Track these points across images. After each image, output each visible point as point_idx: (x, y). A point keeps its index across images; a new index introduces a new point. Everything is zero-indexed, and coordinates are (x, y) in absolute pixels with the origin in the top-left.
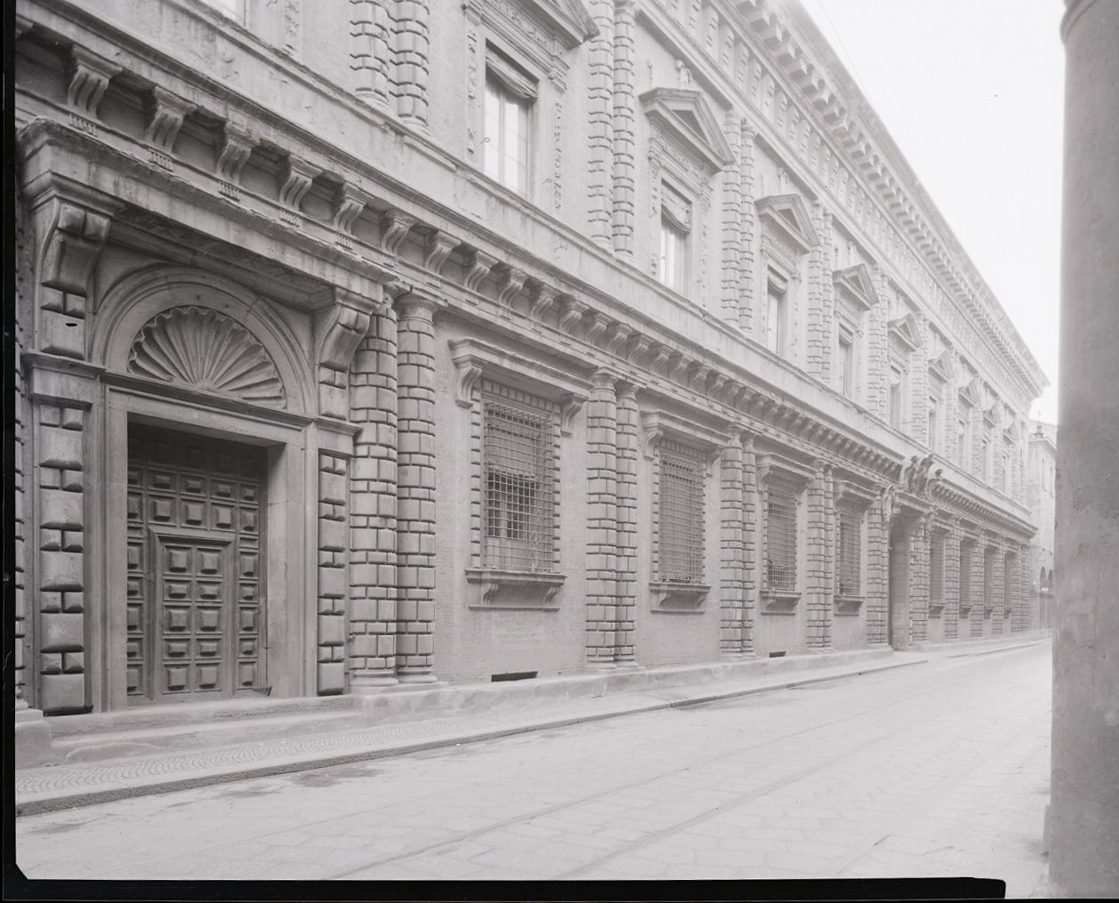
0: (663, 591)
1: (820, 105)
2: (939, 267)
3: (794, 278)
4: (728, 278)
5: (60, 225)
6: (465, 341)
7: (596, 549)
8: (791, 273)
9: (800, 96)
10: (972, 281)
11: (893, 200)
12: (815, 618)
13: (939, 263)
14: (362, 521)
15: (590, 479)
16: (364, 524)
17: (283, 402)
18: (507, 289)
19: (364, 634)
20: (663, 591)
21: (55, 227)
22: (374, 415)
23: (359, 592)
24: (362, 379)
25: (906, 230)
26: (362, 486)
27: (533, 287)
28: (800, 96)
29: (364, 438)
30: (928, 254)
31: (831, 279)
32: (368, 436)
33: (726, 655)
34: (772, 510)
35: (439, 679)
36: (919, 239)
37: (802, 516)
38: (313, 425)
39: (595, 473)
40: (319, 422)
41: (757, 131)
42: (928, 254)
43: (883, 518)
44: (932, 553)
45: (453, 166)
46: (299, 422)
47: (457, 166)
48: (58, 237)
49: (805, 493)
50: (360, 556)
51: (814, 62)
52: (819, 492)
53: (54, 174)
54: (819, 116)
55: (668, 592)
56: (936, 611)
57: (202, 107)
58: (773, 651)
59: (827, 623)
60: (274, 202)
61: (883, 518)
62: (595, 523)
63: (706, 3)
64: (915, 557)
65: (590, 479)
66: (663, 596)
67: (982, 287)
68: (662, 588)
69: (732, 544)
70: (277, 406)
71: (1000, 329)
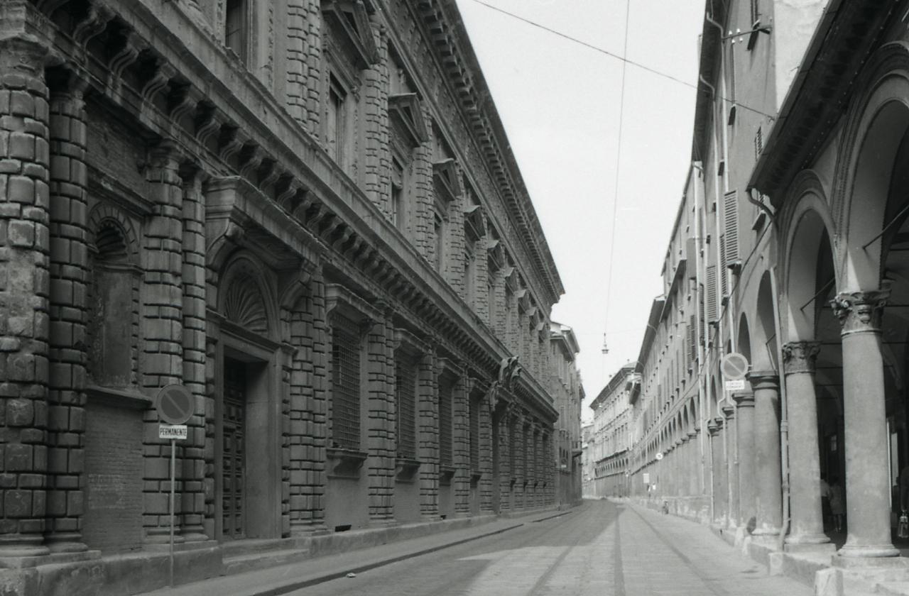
0: (337, 458)
1: (464, 94)
2: (509, 200)
3: (353, 93)
4: (420, 224)
5: (228, 234)
6: (336, 287)
7: (376, 433)
8: (443, 216)
9: (453, 88)
10: (528, 215)
11: (493, 158)
12: (461, 488)
13: (512, 202)
14: (297, 415)
15: (370, 380)
16: (299, 417)
17: (267, 333)
18: (207, 127)
19: (157, 492)
20: (337, 458)
21: (224, 235)
22: (305, 341)
23: (295, 465)
24: (296, 317)
25: (497, 178)
26: (297, 390)
27: (229, 130)
28: (453, 88)
29: (299, 357)
30: (506, 195)
31: (386, 103)
32: (301, 356)
33: (374, 521)
34: (336, 352)
35: (91, 547)
36: (503, 185)
37: (365, 366)
38: (280, 349)
39: (374, 377)
40: (283, 348)
41: (389, 36)
42: (506, 195)
43: (490, 408)
44: (440, 403)
45: (331, 167)
46: (272, 346)
47: (334, 168)
48: (223, 240)
49: (367, 338)
50: (296, 439)
51: (465, 67)
52: (381, 339)
53: (235, 207)
54: (461, 101)
55: (342, 458)
56: (350, 466)
57: (153, 48)
58: (339, 525)
59: (319, 490)
60: (103, 65)
61: (490, 408)
62: (375, 414)
63: (403, 1)
64: (502, 439)
65: (370, 380)
66: (337, 462)
67: (534, 220)
68: (337, 454)
69: (428, 429)
70: (265, 335)
71: (541, 250)
